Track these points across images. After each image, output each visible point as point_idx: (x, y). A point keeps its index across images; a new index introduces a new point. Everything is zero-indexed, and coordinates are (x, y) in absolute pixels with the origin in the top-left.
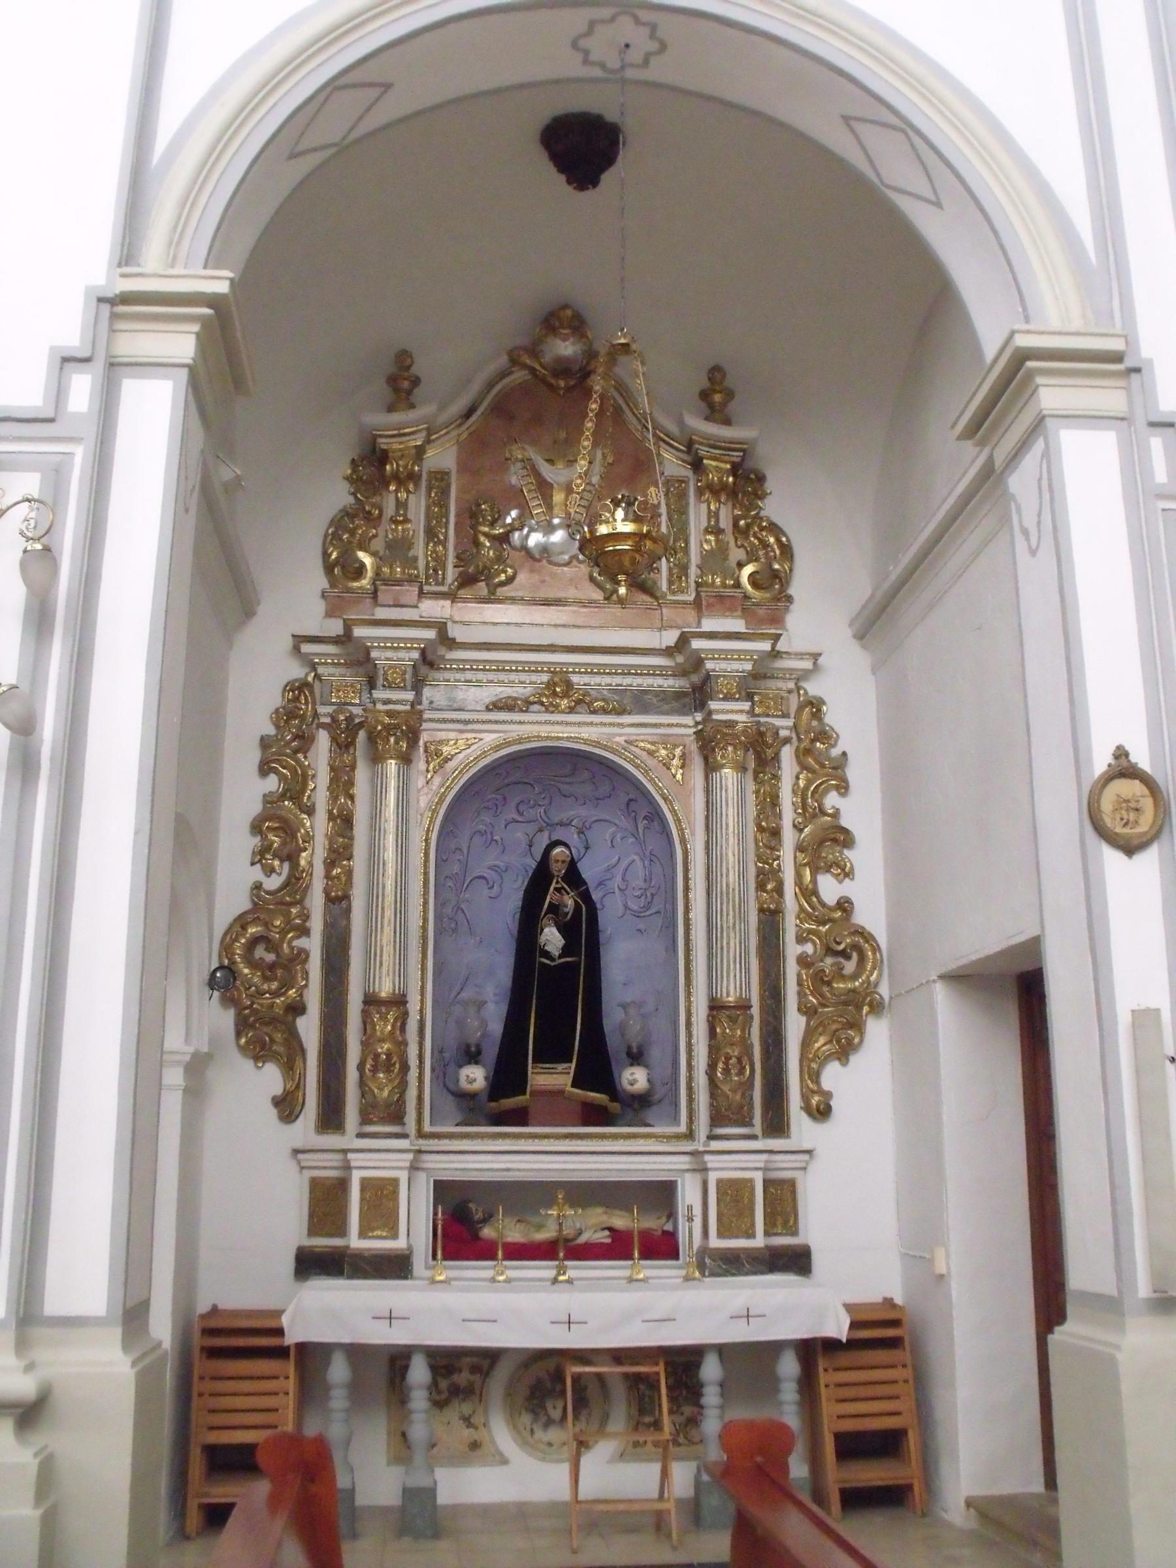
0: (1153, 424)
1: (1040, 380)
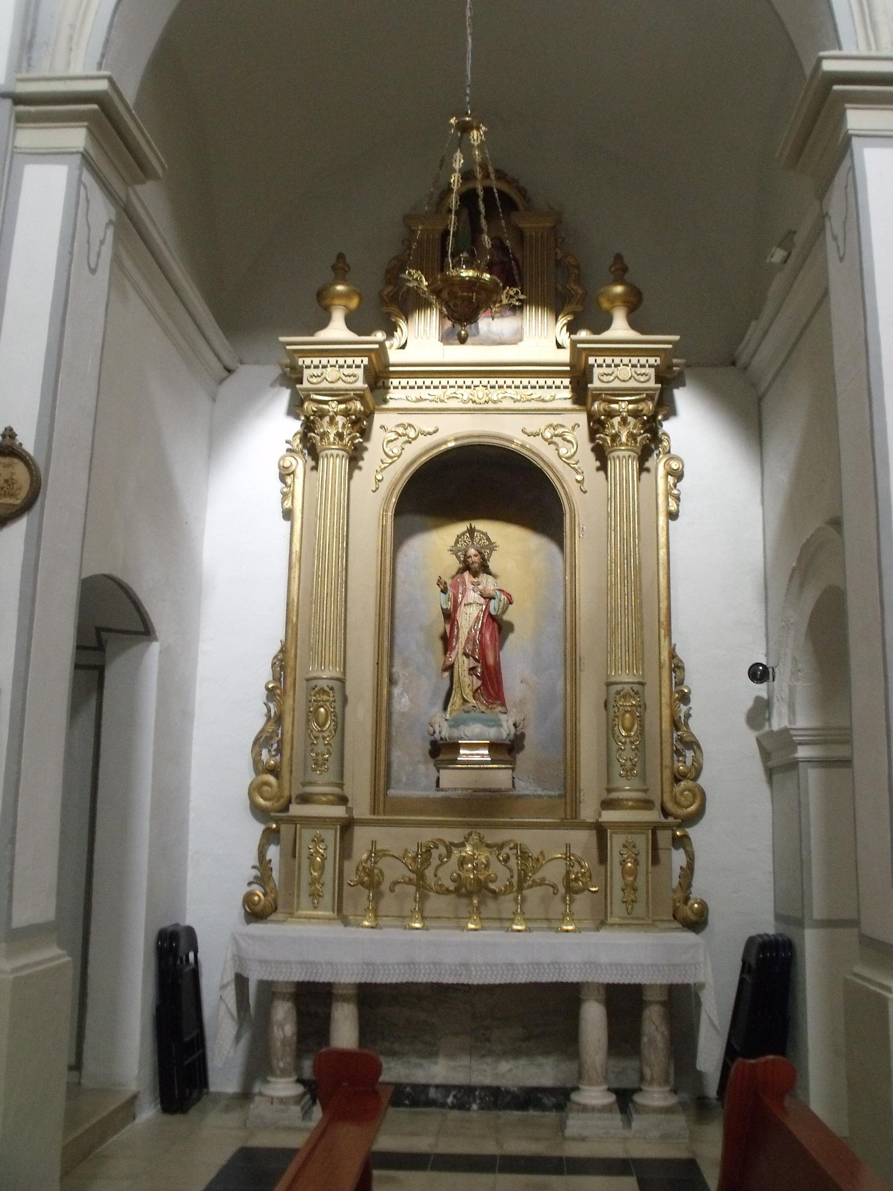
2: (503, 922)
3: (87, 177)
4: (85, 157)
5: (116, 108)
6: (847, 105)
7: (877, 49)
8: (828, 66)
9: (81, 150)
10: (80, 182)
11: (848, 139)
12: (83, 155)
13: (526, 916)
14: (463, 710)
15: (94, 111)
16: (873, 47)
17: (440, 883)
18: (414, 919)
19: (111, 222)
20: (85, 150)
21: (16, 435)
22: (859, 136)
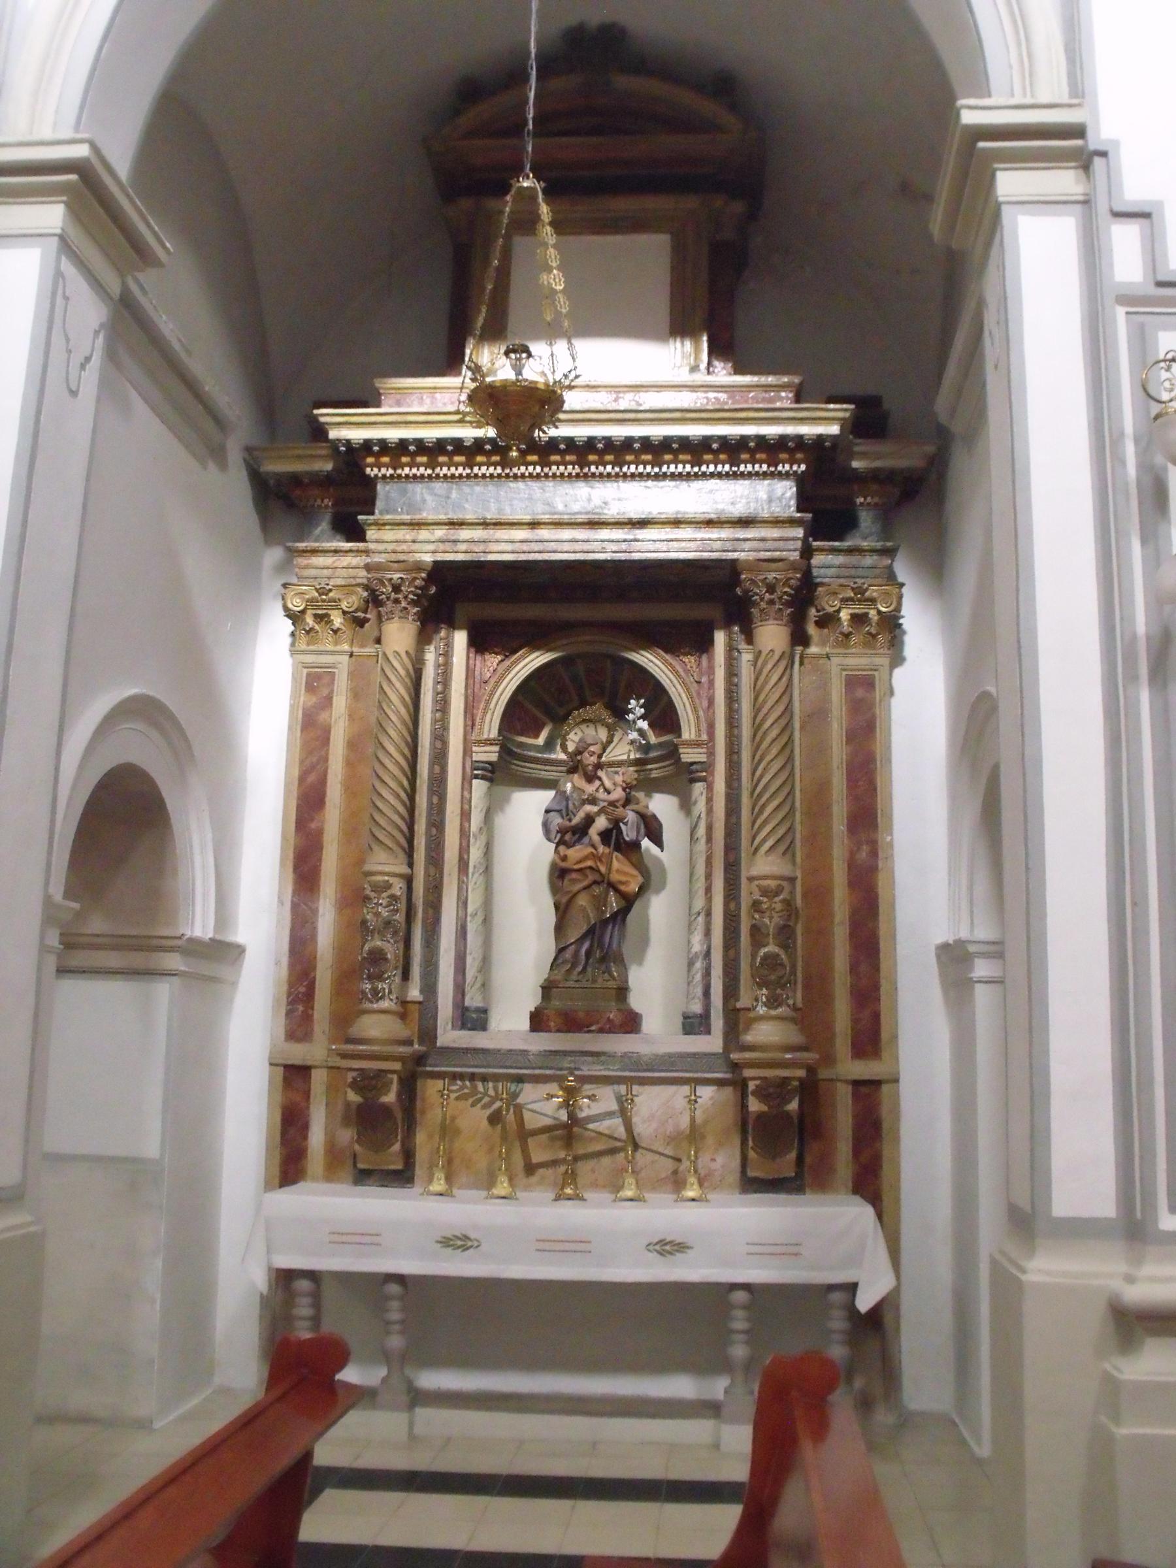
0: (1118, 215)
3: (68, 268)
4: (64, 243)
5: (116, 201)
6: (996, 166)
7: (1032, 96)
8: (968, 118)
9: (58, 231)
10: (59, 275)
11: (998, 206)
16: (1029, 94)
17: (579, 758)
19: (102, 326)
20: (63, 229)
22: (1009, 203)
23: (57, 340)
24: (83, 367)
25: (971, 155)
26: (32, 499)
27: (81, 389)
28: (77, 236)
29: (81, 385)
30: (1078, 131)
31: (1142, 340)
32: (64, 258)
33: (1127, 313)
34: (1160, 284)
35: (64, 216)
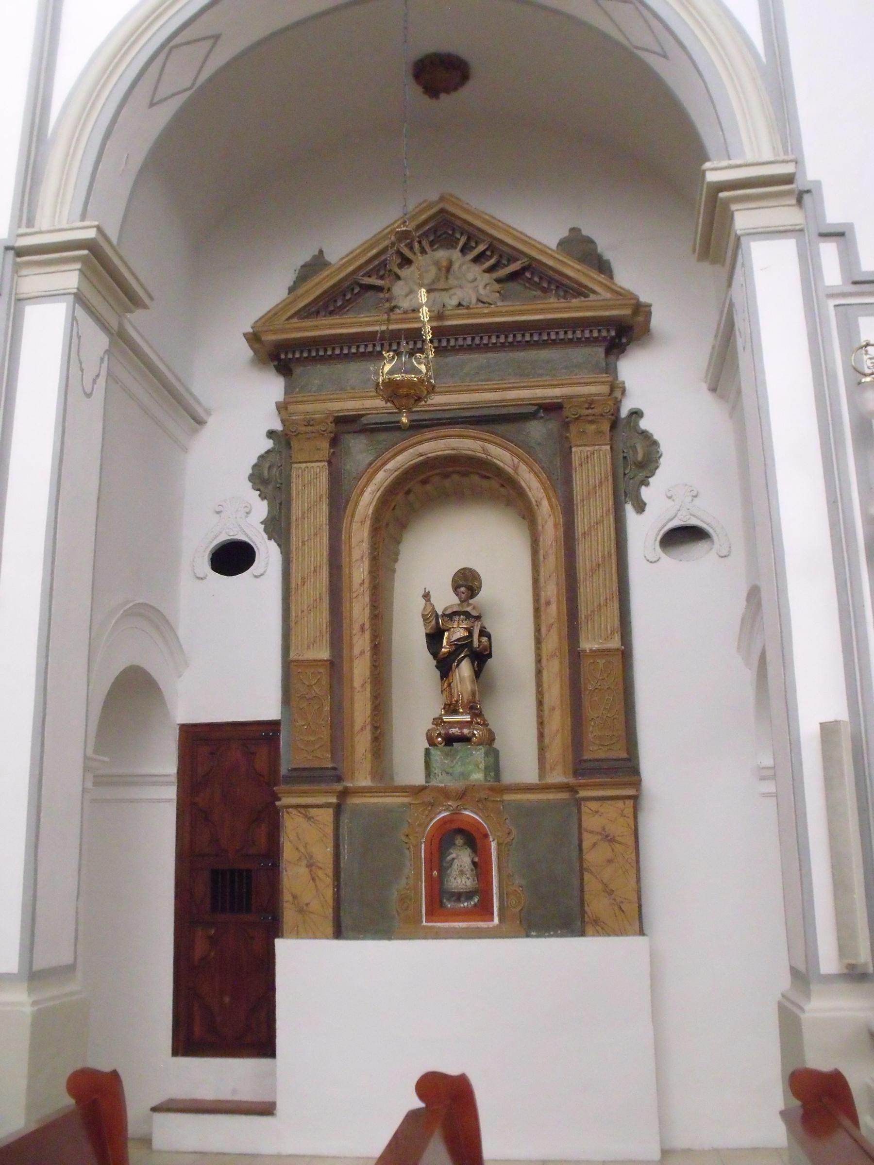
0: (826, 235)
1: (734, 207)
2: (498, 271)
3: (80, 312)
4: (79, 298)
8: (712, 177)
9: (75, 291)
10: (74, 318)
12: (75, 294)
13: (436, 754)
14: (364, 624)
15: (87, 255)
18: (473, 855)
20: (78, 289)
21: (782, 1113)
23: (74, 367)
24: (94, 382)
25: (716, 201)
26: (96, 179)
27: (94, 392)
28: (90, 294)
29: (94, 390)
30: (788, 179)
31: (848, 330)
32: (77, 305)
33: (836, 306)
34: (855, 283)
35: (79, 275)
